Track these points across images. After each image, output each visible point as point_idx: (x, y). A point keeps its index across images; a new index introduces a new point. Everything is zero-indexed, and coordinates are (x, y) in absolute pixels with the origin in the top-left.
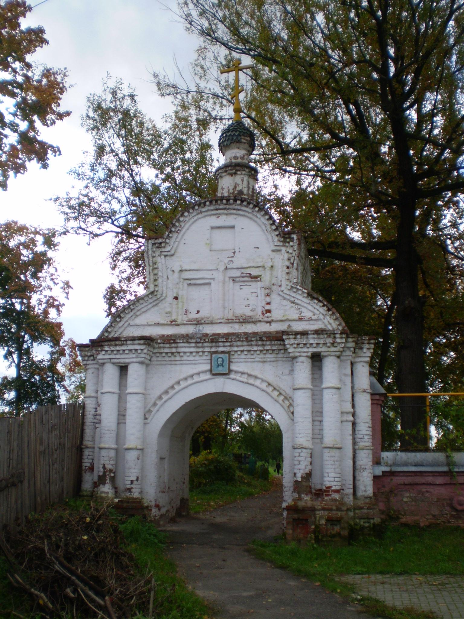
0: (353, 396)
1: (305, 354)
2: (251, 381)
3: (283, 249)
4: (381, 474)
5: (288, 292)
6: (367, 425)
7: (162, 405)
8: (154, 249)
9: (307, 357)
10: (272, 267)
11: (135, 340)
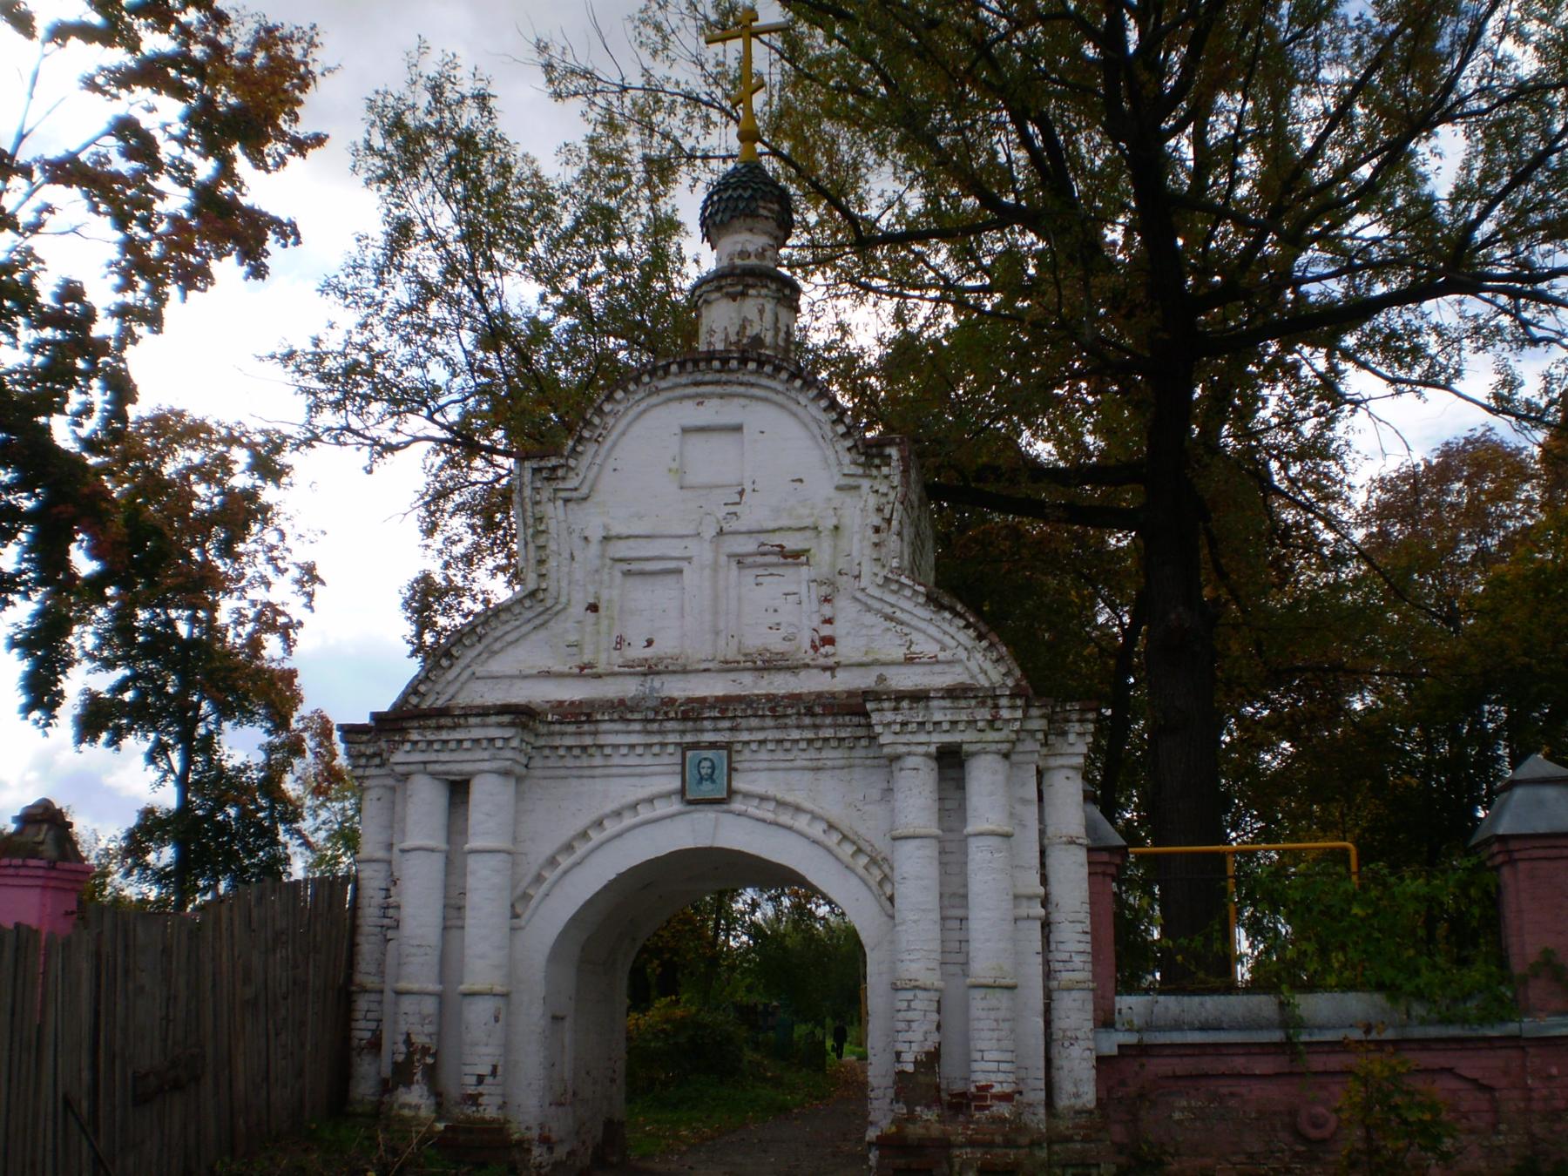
0: (1043, 853)
2: (785, 818)
4: (1115, 1051)
5: (877, 593)
6: (1079, 927)
7: (556, 882)
8: (539, 484)
10: (836, 528)
11: (488, 715)
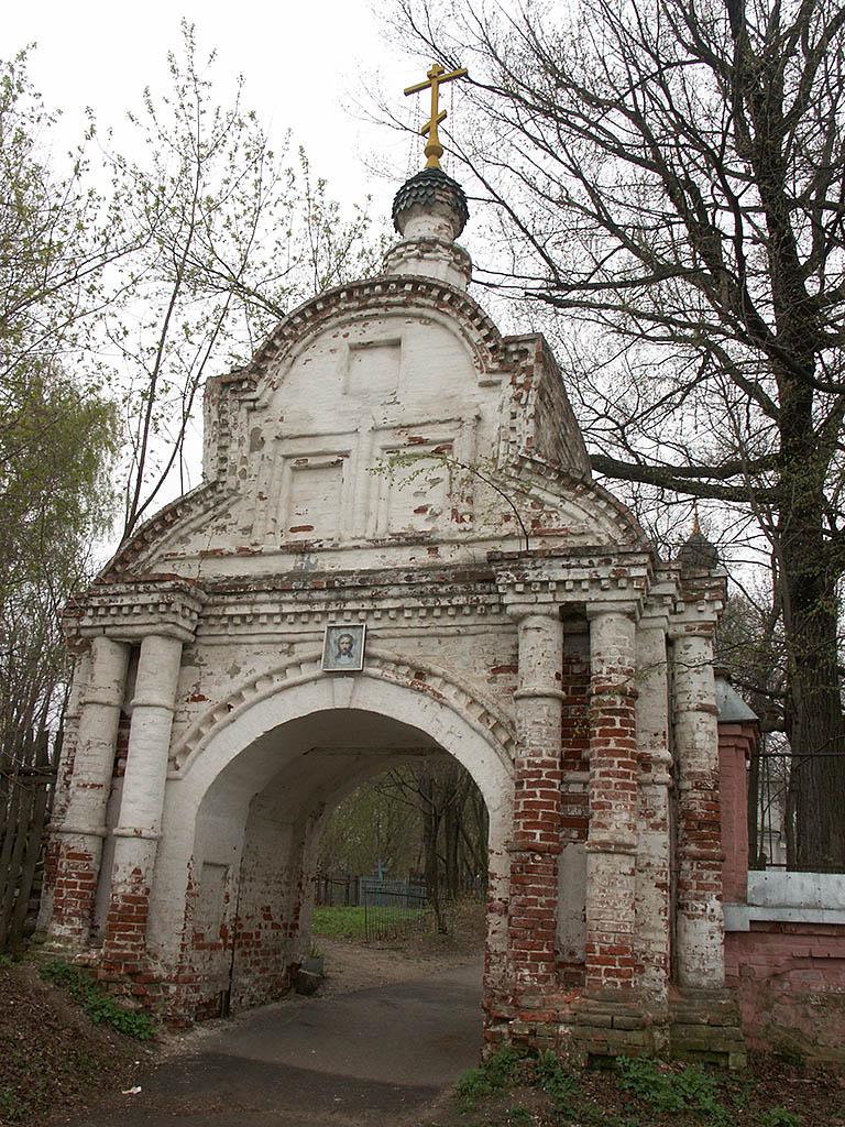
1: (545, 609)
3: (507, 379)
9: (547, 615)
10: (478, 418)
